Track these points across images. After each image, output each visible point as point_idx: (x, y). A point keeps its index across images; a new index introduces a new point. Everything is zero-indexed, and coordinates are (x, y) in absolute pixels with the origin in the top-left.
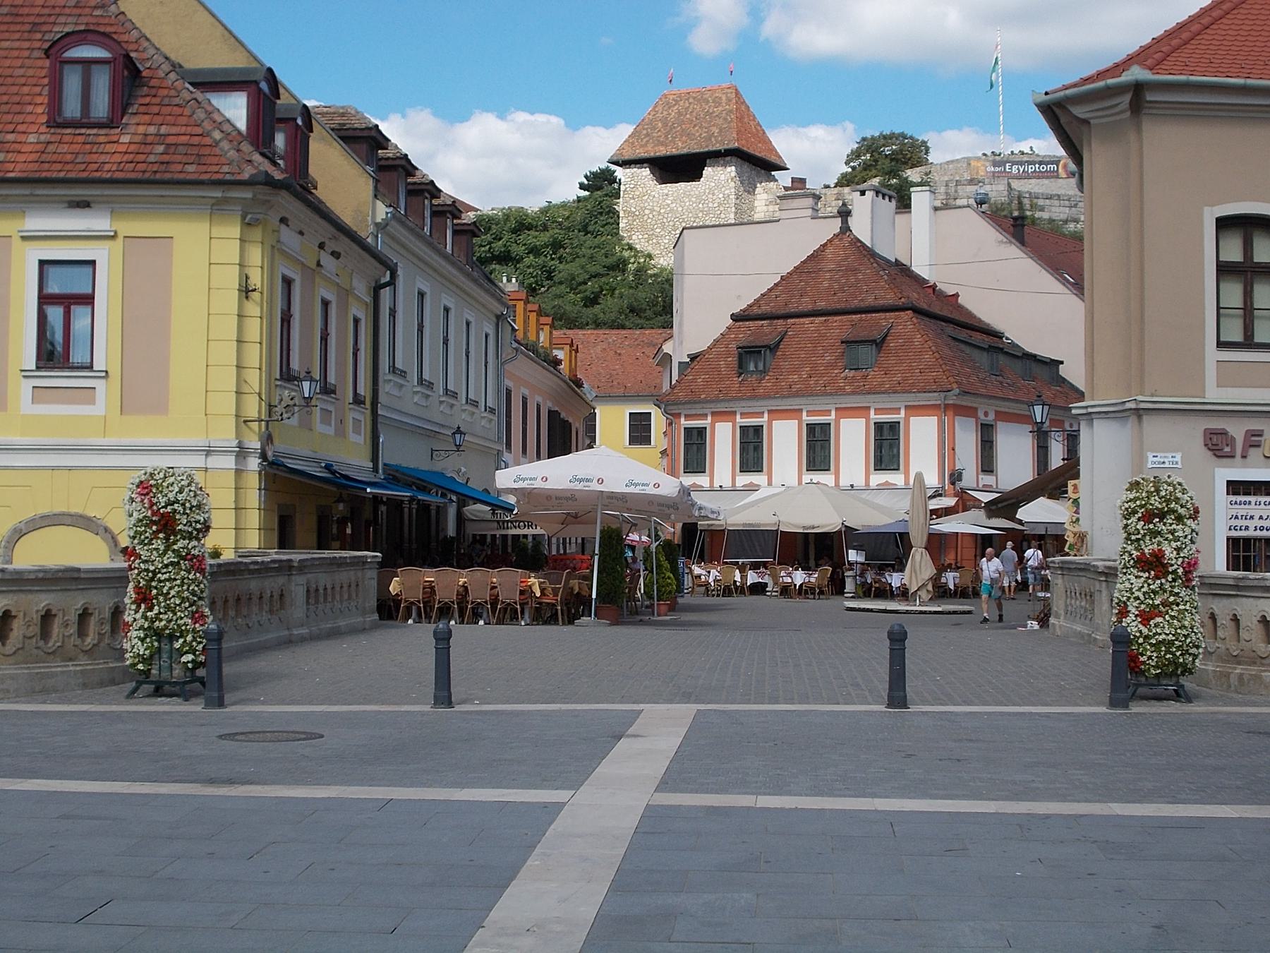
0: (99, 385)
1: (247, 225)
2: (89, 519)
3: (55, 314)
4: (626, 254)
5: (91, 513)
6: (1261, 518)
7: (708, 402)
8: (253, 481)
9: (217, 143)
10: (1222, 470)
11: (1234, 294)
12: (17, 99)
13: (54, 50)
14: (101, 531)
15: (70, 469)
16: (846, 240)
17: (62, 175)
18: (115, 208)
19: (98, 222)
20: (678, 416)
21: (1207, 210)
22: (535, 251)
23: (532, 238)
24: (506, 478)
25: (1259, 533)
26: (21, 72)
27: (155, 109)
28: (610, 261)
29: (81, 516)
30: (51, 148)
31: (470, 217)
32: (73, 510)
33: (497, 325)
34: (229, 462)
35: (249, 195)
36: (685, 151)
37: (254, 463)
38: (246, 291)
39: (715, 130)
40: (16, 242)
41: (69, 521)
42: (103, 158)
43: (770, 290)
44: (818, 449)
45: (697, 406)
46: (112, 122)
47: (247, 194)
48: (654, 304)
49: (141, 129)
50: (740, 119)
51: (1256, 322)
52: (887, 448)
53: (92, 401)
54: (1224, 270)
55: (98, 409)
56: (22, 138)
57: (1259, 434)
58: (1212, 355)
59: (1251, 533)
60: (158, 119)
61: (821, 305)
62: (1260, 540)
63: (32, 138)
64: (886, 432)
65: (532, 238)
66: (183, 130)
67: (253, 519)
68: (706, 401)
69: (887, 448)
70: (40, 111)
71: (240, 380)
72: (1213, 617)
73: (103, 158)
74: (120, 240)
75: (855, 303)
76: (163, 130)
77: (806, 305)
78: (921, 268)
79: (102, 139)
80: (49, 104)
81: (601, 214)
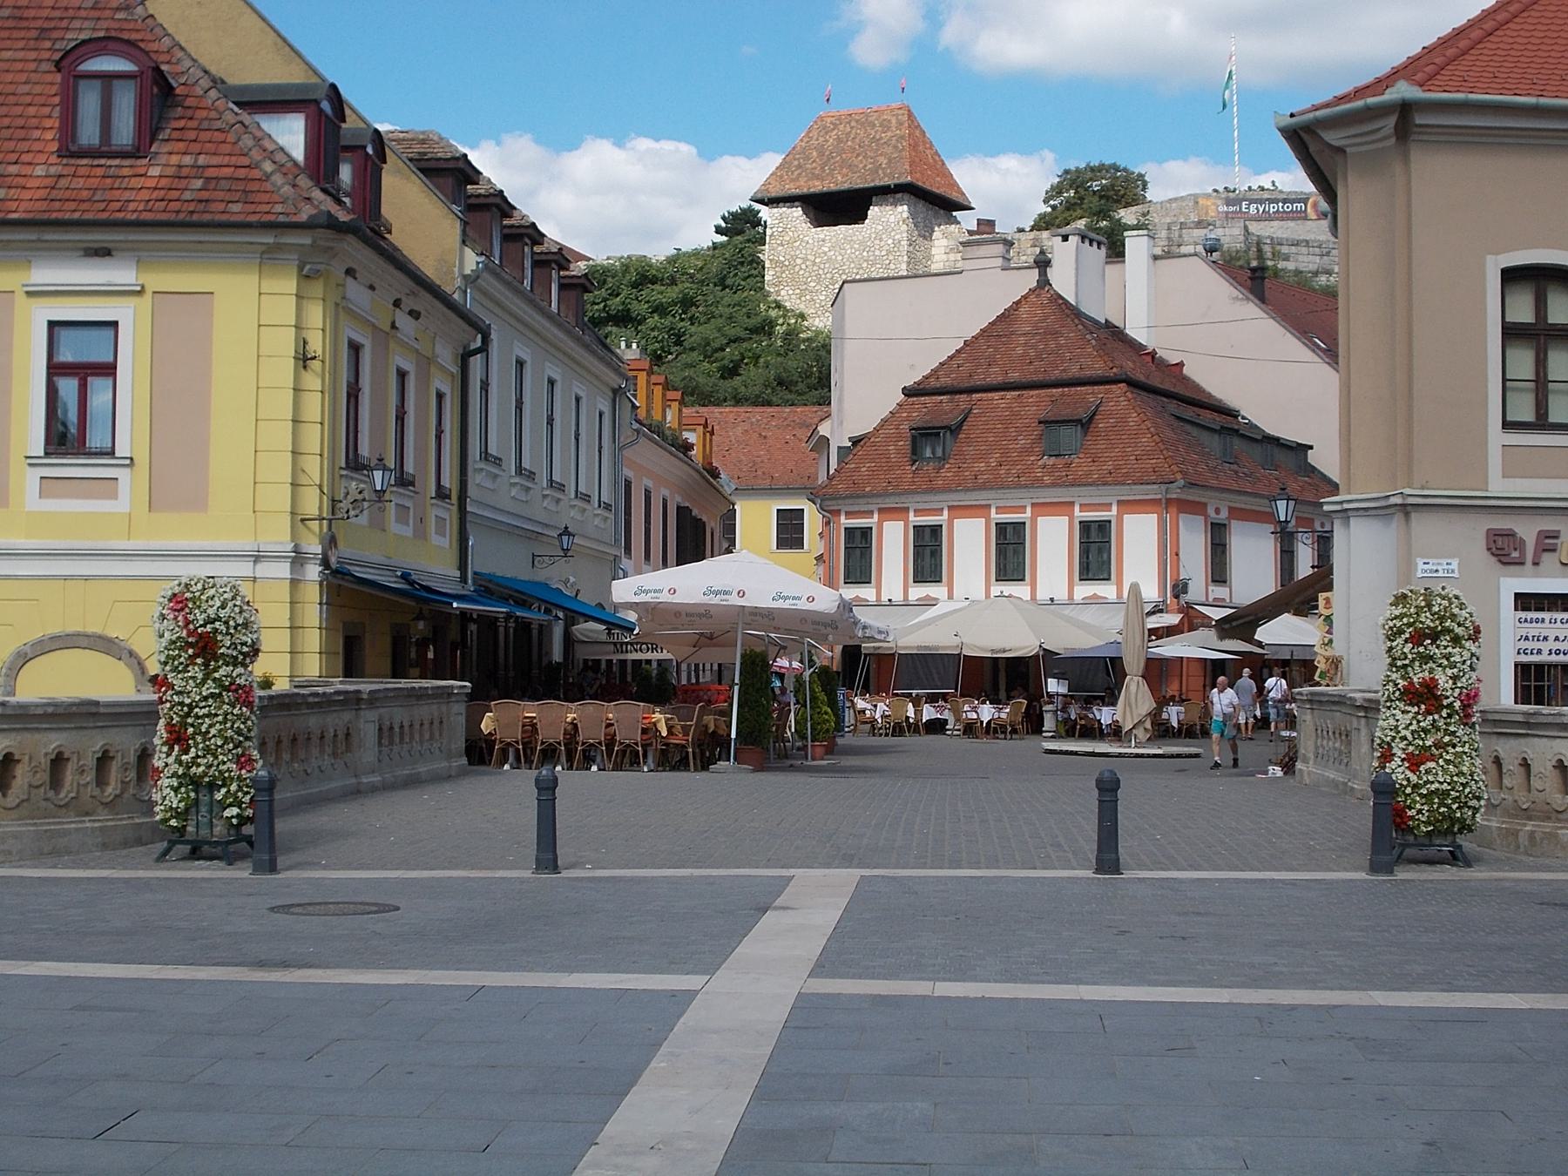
0: (123, 475)
1: (305, 277)
2: (110, 641)
3: (68, 387)
4: (773, 313)
5: (112, 633)
6: (1557, 639)
7: (874, 496)
8: (312, 594)
9: (268, 177)
10: (1509, 580)
11: (1523, 362)
12: (21, 122)
13: (66, 62)
14: (125, 655)
15: (87, 578)
16: (1045, 296)
17: (76, 216)
18: (142, 257)
19: (121, 274)
20: (837, 513)
21: (1490, 259)
22: (660, 310)
23: (657, 294)
24: (624, 590)
25: (1554, 658)
26: (26, 88)
27: (192, 135)
28: (753, 322)
29: (100, 637)
30: (63, 183)
31: (580, 268)
32: (90, 630)
33: (614, 401)
34: (283, 570)
35: (307, 241)
36: (846, 186)
37: (313, 572)
38: (303, 359)
39: (883, 161)
40: (20, 298)
41: (85, 643)
42: (127, 195)
43: (951, 358)
44: (1010, 553)
45: (861, 501)
46: (138, 151)
47: (305, 239)
48: (808, 376)
49: (174, 159)
50: (914, 147)
51: (1551, 398)
52: (1095, 553)
53: (113, 495)
54: (1511, 333)
55: (121, 505)
56: (27, 170)
57: (1555, 535)
58: (1497, 438)
59: (1544, 658)
60: (196, 147)
61: (1014, 376)
62: (1556, 666)
63: (39, 171)
64: (1094, 533)
65: (657, 294)
66: (226, 160)
67: (313, 640)
68: (871, 495)
69: (1095, 553)
70: (50, 137)
71: (296, 470)
72: (1497, 761)
73: (127, 195)
74: (148, 296)
75: (1056, 374)
76: (202, 160)
77: (995, 376)
78: (1137, 330)
79: (126, 172)
80: (60, 129)
81: (742, 263)
